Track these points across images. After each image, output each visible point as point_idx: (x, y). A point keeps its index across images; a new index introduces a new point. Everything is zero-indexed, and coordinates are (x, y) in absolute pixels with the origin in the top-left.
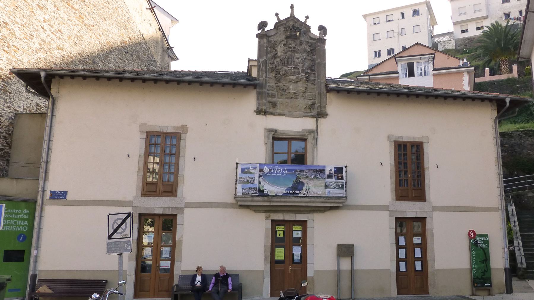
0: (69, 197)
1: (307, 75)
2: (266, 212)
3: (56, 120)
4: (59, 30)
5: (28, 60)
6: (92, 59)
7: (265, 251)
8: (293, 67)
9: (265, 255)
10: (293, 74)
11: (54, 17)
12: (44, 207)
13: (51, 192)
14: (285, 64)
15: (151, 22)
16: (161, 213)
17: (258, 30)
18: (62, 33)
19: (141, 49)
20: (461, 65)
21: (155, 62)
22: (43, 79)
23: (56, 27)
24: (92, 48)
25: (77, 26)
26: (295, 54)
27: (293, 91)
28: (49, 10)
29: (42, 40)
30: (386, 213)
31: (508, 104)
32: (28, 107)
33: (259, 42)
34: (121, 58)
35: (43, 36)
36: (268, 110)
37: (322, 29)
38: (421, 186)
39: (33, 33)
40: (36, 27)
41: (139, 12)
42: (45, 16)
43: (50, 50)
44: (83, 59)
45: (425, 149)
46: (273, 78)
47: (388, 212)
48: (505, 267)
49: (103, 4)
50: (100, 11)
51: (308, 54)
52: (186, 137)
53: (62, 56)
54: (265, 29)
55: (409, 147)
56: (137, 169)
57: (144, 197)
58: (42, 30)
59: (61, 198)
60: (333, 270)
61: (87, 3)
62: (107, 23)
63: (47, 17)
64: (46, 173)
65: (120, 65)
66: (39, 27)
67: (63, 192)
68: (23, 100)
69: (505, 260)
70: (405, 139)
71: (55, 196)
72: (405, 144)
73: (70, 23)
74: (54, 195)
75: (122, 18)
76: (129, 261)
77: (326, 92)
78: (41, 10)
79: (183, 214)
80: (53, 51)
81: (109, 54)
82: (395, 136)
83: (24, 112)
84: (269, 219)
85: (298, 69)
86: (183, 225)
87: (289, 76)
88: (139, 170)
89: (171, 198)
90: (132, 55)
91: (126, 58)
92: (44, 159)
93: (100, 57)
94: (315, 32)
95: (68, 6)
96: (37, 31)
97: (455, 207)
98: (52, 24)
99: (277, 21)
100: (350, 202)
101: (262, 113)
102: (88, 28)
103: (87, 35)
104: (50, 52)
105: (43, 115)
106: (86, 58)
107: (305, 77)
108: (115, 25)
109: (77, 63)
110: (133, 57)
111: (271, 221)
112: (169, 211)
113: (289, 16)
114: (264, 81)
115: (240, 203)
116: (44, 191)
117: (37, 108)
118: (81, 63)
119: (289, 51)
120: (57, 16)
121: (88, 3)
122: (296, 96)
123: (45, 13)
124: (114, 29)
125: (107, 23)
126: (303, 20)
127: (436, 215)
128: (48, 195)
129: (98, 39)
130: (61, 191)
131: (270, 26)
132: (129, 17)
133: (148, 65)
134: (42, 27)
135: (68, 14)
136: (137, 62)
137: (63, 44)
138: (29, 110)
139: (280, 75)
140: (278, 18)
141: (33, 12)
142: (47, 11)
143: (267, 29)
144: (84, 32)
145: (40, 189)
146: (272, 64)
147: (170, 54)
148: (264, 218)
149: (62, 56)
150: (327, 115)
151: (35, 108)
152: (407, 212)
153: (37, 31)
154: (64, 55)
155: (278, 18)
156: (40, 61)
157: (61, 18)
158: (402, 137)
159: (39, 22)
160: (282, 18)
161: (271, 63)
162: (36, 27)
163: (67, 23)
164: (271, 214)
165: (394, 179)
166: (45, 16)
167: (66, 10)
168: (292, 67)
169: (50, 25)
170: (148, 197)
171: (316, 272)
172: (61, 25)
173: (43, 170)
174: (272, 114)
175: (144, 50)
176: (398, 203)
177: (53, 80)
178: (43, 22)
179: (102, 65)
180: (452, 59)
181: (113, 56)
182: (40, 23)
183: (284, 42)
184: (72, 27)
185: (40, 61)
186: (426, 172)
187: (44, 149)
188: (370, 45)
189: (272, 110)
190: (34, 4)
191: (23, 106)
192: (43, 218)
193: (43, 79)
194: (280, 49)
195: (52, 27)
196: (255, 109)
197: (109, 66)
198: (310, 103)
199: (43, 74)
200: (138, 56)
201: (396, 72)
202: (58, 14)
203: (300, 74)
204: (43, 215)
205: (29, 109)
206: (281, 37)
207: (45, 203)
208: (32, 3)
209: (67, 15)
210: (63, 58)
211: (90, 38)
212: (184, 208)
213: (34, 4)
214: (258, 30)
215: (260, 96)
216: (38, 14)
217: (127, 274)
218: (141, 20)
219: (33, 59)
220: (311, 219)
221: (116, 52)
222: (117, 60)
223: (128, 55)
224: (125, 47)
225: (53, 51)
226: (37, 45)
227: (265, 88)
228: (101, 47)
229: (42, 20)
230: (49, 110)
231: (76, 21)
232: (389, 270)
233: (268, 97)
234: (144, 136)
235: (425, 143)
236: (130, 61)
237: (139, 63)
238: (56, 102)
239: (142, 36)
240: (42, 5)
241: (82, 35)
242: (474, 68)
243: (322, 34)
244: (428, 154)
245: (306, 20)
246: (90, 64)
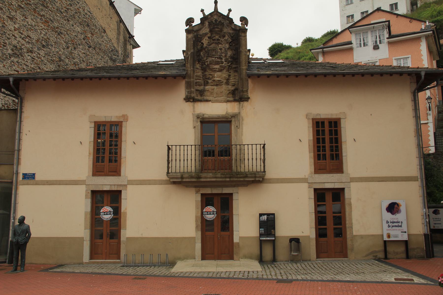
0: (37, 178)
1: (230, 64)
2: (195, 187)
3: (24, 115)
4: (28, 36)
5: (3, 64)
6: (58, 57)
7: (196, 221)
8: (217, 57)
9: (196, 224)
10: (217, 63)
11: (23, 25)
12: (18, 186)
13: (23, 174)
14: (210, 55)
15: (111, 16)
16: (108, 189)
17: (187, 26)
18: (30, 38)
19: (103, 42)
20: (423, 28)
21: (117, 51)
22: (11, 83)
23: (25, 33)
24: (58, 47)
25: (43, 30)
26: (218, 45)
27: (217, 79)
28: (18, 19)
29: (14, 46)
30: (306, 185)
31: (423, 77)
32: (6, 104)
33: (187, 37)
34: (85, 52)
35: (15, 42)
36: (196, 98)
37: (244, 20)
38: (339, 160)
39: (6, 41)
40: (8, 36)
41: (99, 9)
42: (15, 26)
43: (21, 54)
44: (51, 58)
45: (342, 125)
46: (200, 68)
47: (307, 184)
48: (424, 233)
49: (65, 7)
50: (64, 14)
51: (230, 44)
52: (126, 125)
53: (32, 58)
54: (192, 25)
55: (327, 124)
56: (88, 153)
57: (94, 177)
58: (14, 37)
59: (31, 179)
60: (256, 237)
61: (51, 8)
62: (71, 23)
63: (17, 26)
64: (19, 159)
65: (84, 59)
66: (11, 36)
67: (32, 174)
68: (1, 99)
69: (425, 226)
70: (322, 117)
71: (26, 177)
72: (323, 121)
73: (38, 28)
74: (25, 176)
75: (84, 16)
76: (85, 229)
77: (248, 77)
78: (11, 20)
79: (126, 190)
80: (24, 54)
81: (74, 51)
82: (314, 114)
83: (3, 109)
84: (199, 193)
85: (222, 59)
86: (126, 199)
87: (213, 65)
88: (90, 154)
89: (116, 177)
90: (94, 48)
91: (90, 52)
92: (16, 148)
93: (65, 54)
94: (238, 22)
95: (34, 14)
96: (9, 39)
97: (392, 177)
98: (21, 32)
99: (202, 16)
100: (269, 175)
101: (190, 100)
102: (54, 30)
103: (52, 36)
104: (21, 55)
105: (15, 110)
106: (53, 57)
107: (228, 65)
108: (78, 24)
109: (46, 62)
110: (95, 50)
111: (200, 194)
112: (115, 188)
113: (213, 11)
114: (192, 72)
115: (172, 180)
116: (17, 173)
117: (13, 104)
118: (49, 62)
119: (213, 43)
120: (26, 23)
121: (52, 9)
122: (221, 83)
123: (15, 23)
124: (77, 27)
125: (71, 23)
126: (225, 13)
127: (353, 185)
128: (21, 177)
129: (63, 38)
130: (30, 174)
131: (197, 22)
132: (90, 14)
133: (110, 55)
134: (13, 35)
135: (35, 21)
136: (100, 54)
137: (32, 48)
138: (7, 107)
139: (206, 65)
140: (204, 14)
141: (4, 23)
142: (17, 21)
143: (194, 24)
144: (50, 35)
145: (15, 172)
146: (198, 56)
147: (132, 42)
148: (195, 192)
149: (32, 58)
150: (249, 98)
151: (12, 104)
152: (325, 183)
153: (9, 39)
154: (34, 56)
155: (204, 14)
156: (13, 64)
157: (29, 25)
158: (320, 114)
159: (11, 31)
160: (207, 13)
161: (198, 55)
162: (8, 36)
163: (34, 29)
164: (201, 189)
165: (312, 154)
166: (15, 26)
167: (33, 17)
168: (216, 58)
169: (20, 33)
170: (98, 177)
171: (241, 238)
172: (29, 31)
173: (16, 156)
174: (200, 101)
175: (106, 42)
176: (317, 176)
177: (21, 83)
178: (14, 30)
179: (68, 61)
180: (415, 23)
181: (77, 52)
182: (11, 32)
183: (209, 35)
184: (39, 31)
185: (13, 64)
186: (344, 146)
187: (16, 139)
188: (342, 10)
189: (199, 98)
190: (5, 17)
191: (2, 103)
192: (18, 195)
193: (11, 83)
194: (205, 41)
195: (22, 34)
196: (184, 97)
197: (74, 61)
198: (233, 88)
199: (11, 80)
200: (101, 48)
201: (350, 43)
202: (26, 22)
203: (223, 62)
204: (18, 193)
205: (7, 105)
206: (206, 30)
207: (19, 183)
208: (3, 16)
209: (34, 22)
210: (33, 59)
211: (56, 39)
212: (127, 185)
213: (5, 17)
214: (187, 26)
215: (189, 86)
216: (9, 25)
217: (84, 240)
218: (102, 15)
219: (8, 63)
220: (236, 192)
221: (79, 48)
222: (81, 55)
223: (91, 49)
224: (88, 42)
225: (24, 54)
226: (10, 51)
227: (193, 78)
228: (66, 45)
229: (13, 28)
230: (19, 107)
231: (42, 25)
232: (309, 237)
233: (196, 86)
234: (93, 125)
235: (342, 119)
236: (93, 54)
237: (102, 55)
238: (24, 101)
239: (104, 30)
240: (12, 16)
241: (49, 37)
242: (432, 32)
243: (244, 25)
244: (345, 129)
245: (229, 13)
246: (56, 61)
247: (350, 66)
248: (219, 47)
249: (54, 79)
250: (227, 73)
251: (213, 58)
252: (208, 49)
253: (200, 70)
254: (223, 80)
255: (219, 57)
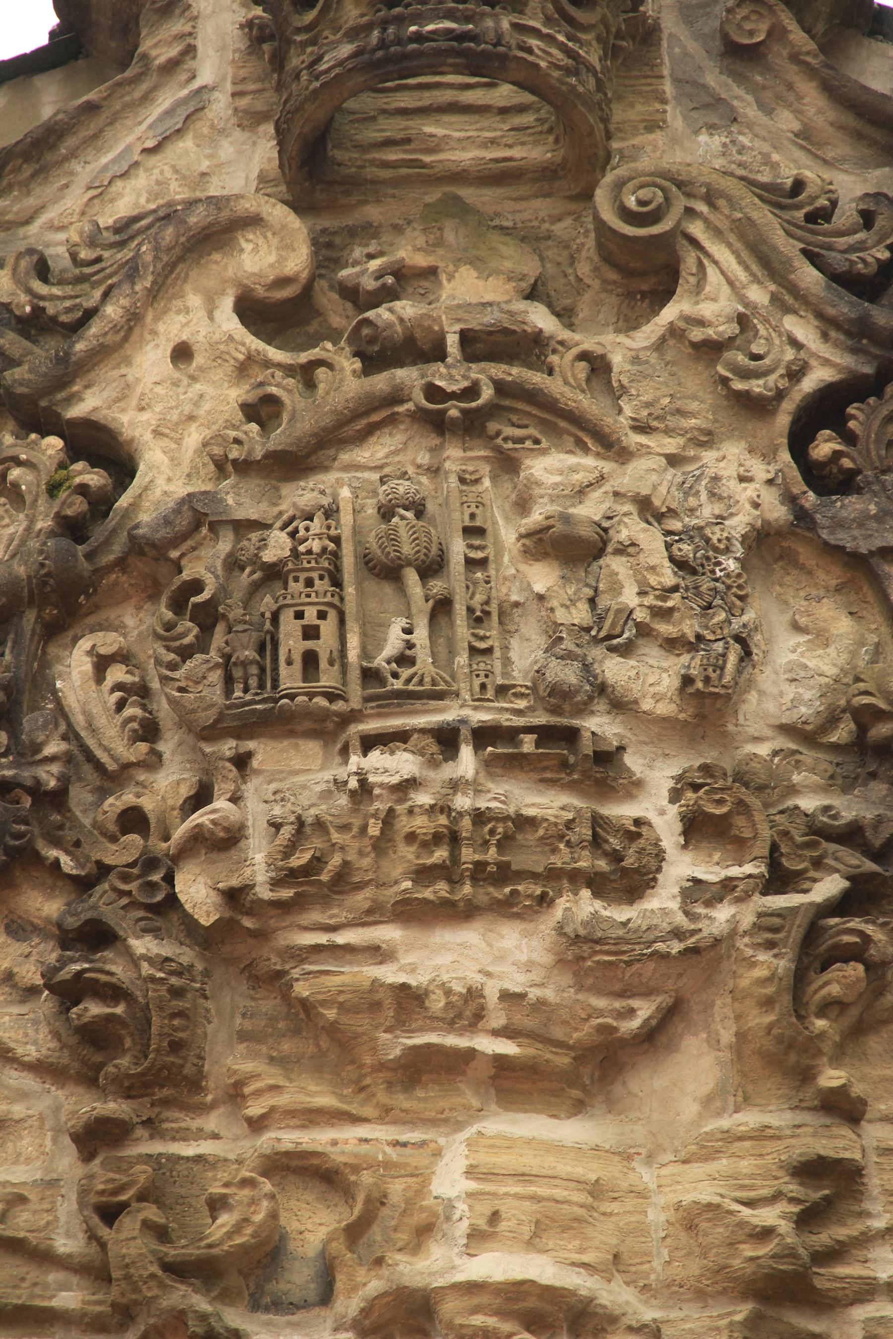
232: (620, 594)
247: (754, 180)
248: (523, 506)
249: (85, 142)
250: (750, 1119)
251: (368, 743)
252: (233, 564)
253: (38, 1068)
254: (649, 1314)
255: (545, 734)
